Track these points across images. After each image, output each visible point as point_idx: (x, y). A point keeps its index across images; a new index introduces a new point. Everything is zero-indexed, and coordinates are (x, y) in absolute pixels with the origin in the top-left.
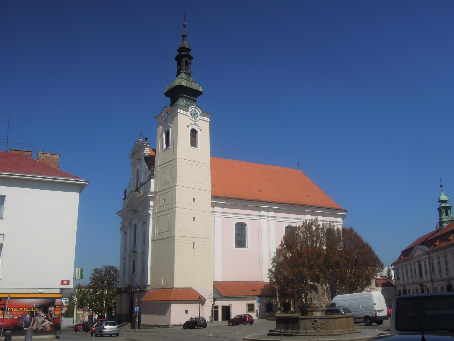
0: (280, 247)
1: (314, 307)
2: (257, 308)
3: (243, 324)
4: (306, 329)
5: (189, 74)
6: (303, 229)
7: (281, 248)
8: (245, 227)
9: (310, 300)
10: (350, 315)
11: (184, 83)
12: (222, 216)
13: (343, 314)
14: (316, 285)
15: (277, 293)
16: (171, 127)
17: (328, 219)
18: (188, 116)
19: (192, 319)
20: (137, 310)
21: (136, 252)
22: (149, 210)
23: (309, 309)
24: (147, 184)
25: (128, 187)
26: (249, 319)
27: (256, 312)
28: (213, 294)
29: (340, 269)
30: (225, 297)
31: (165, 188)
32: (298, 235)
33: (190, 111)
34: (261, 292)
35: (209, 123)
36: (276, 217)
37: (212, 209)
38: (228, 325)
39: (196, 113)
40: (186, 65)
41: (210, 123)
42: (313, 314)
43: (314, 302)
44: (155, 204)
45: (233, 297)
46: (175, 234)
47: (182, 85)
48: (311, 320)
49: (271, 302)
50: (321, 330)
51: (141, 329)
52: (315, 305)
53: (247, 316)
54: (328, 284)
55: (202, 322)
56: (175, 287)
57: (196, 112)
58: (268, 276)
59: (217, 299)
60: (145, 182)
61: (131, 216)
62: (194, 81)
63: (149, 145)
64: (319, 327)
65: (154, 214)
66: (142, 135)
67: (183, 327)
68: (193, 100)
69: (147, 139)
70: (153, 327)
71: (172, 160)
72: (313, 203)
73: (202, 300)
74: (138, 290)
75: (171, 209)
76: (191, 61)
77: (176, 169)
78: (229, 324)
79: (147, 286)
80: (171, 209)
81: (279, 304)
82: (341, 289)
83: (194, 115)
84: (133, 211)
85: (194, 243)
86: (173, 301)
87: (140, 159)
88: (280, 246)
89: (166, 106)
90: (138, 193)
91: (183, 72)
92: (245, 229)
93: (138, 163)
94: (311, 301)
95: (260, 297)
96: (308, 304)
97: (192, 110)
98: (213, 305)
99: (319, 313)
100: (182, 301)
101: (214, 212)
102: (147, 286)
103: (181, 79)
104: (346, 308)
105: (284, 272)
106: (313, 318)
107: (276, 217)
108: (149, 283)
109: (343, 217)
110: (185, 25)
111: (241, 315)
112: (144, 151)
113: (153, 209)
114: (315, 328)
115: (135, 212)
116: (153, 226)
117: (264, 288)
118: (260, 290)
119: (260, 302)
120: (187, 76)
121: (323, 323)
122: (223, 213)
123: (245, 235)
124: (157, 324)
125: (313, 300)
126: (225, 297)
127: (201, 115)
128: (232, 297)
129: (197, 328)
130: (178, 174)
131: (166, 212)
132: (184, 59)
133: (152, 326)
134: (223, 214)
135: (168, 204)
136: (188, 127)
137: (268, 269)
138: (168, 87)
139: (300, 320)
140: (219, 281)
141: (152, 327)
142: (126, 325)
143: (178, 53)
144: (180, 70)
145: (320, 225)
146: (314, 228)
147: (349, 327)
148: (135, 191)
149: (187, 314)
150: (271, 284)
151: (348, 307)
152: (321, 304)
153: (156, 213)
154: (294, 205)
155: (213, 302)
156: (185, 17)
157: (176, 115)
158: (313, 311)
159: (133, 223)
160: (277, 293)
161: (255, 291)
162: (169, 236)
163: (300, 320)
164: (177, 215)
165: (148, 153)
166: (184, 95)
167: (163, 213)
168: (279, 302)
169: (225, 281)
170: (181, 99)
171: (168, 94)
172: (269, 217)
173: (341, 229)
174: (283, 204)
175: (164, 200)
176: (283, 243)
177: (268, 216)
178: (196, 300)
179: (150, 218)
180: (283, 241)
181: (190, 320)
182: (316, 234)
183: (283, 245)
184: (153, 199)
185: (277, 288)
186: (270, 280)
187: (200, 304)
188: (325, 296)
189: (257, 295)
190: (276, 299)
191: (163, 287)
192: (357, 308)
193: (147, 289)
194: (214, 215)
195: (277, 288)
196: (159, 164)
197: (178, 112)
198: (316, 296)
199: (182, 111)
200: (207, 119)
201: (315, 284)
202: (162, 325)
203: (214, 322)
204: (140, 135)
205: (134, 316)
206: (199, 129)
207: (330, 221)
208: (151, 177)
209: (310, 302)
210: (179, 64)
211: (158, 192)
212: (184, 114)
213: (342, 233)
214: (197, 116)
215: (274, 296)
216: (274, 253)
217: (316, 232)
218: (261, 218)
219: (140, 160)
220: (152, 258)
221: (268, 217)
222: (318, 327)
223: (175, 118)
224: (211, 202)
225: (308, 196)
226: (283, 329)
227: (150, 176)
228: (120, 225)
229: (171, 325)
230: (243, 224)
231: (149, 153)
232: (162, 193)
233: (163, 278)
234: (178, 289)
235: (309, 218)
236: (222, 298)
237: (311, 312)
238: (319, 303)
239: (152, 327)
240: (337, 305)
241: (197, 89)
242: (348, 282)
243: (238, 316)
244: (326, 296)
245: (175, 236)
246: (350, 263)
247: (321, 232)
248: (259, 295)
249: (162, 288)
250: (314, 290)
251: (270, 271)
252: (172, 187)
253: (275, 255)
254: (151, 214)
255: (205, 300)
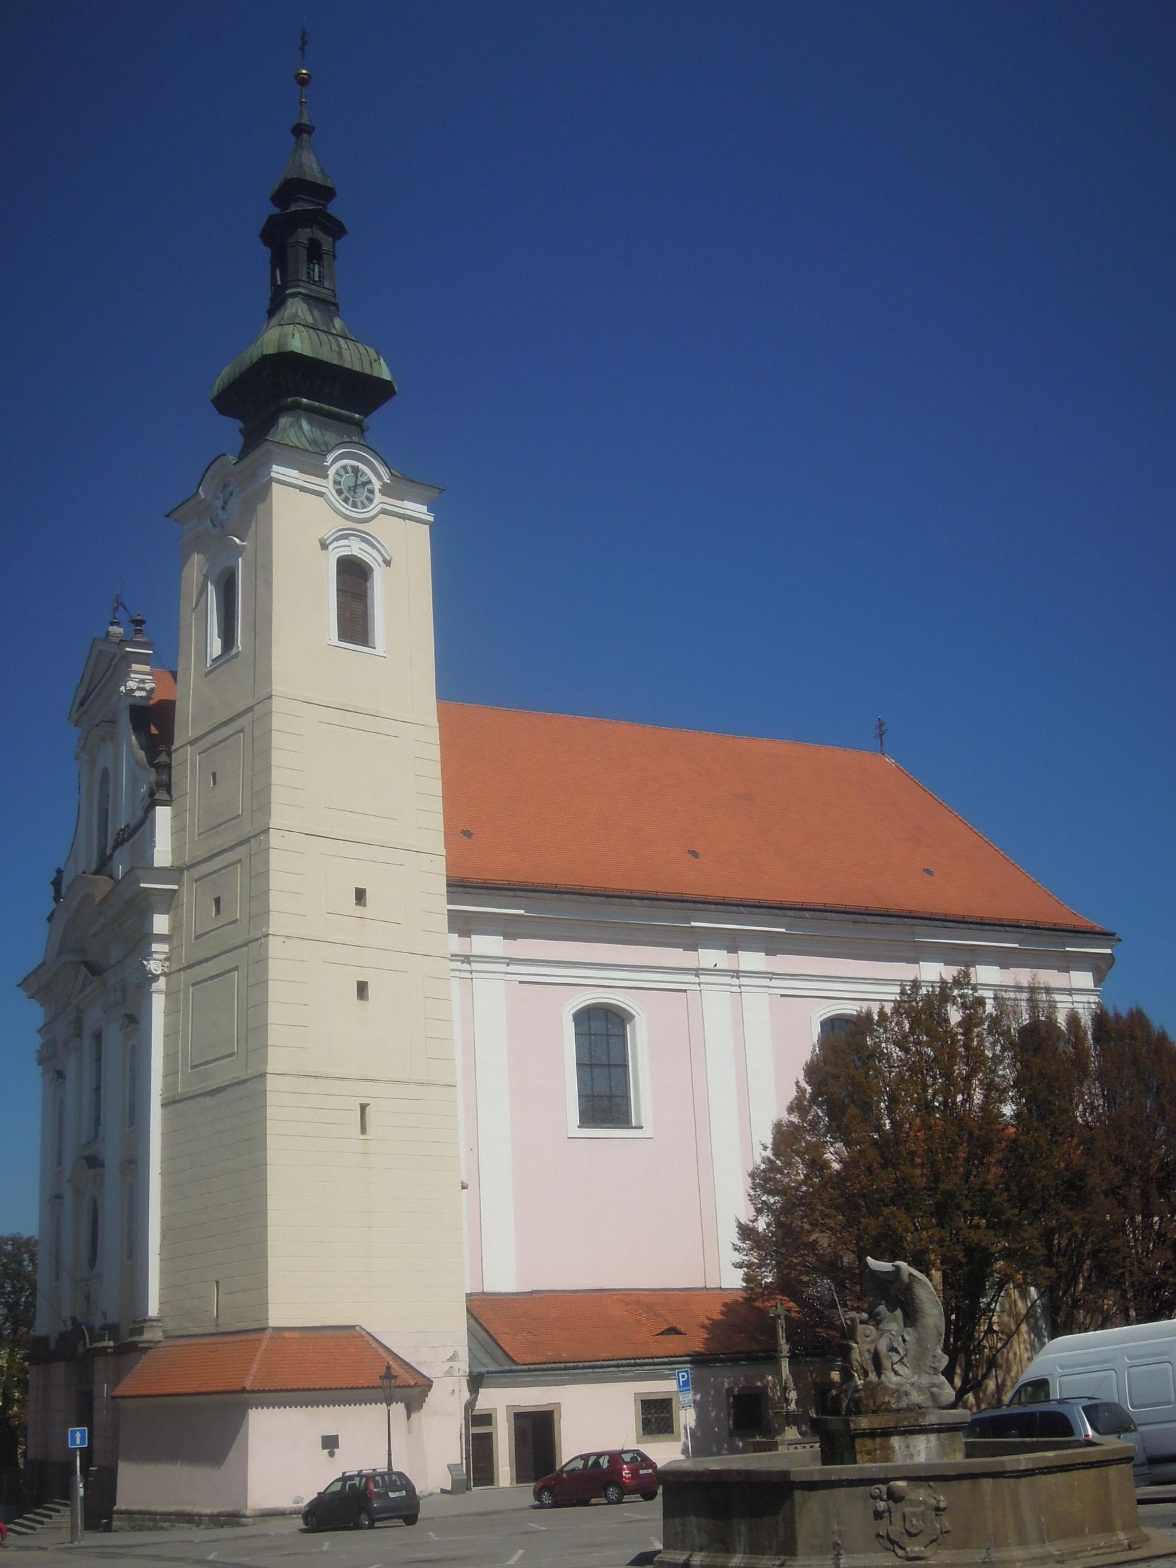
0: (789, 1113)
1: (894, 1406)
2: (686, 1417)
3: (606, 1497)
4: (836, 1546)
5: (326, 305)
6: (899, 1024)
7: (795, 1119)
8: (624, 1029)
9: (870, 1367)
10: (1115, 1451)
11: (299, 343)
12: (509, 977)
13: (1089, 1443)
14: (905, 1278)
15: (783, 1341)
16: (239, 551)
17: (1023, 976)
18: (321, 494)
19: (344, 1479)
20: (78, 1442)
21: (101, 1164)
22: (149, 955)
23: (864, 1423)
24: (139, 833)
25: (68, 859)
26: (634, 1472)
27: (683, 1439)
28: (464, 1355)
29: (1089, 1208)
30: (525, 1367)
31: (219, 842)
32: (876, 1053)
33: (331, 472)
34: (707, 1339)
35: (428, 526)
36: (772, 975)
37: (455, 943)
38: (534, 1507)
39: (364, 484)
40: (310, 260)
41: (435, 529)
42: (892, 1449)
43: (895, 1379)
44: (175, 927)
45: (566, 1369)
46: (266, 1063)
47: (293, 353)
48: (868, 1489)
49: (759, 1384)
50: (928, 1552)
51: (115, 1531)
52: (898, 1393)
53: (627, 1458)
54: (1032, 1289)
55: (392, 1495)
56: (270, 1325)
57: (364, 479)
58: (738, 1257)
59: (485, 1381)
60: (133, 823)
61: (81, 992)
62: (349, 336)
63: (151, 652)
64: (916, 1535)
65: (174, 972)
66: (120, 606)
67: (306, 1524)
68: (349, 421)
69: (140, 623)
70: (170, 1521)
71: (250, 709)
72: (953, 902)
73: (410, 1386)
74: (111, 1344)
75: (246, 945)
76: (334, 241)
77: (267, 751)
78: (537, 1503)
79: (145, 1321)
80: (246, 945)
81: (793, 1395)
82: (1100, 1309)
83: (354, 489)
84: (84, 971)
85: (363, 1108)
86: (259, 1391)
87: (112, 722)
88: (790, 1110)
89: (219, 457)
90: (107, 878)
91: (300, 293)
92: (624, 1036)
93: (103, 739)
94: (879, 1374)
95: (698, 1360)
96: (857, 1390)
97: (344, 468)
98: (470, 1405)
99: (928, 1441)
100: (304, 1390)
101: (467, 959)
102: (145, 1321)
103: (286, 327)
104: (1109, 1406)
105: (813, 1237)
106: (882, 1476)
107: (772, 975)
108: (153, 1310)
109: (1101, 968)
110: (303, 82)
111: (599, 1455)
112: (125, 678)
113: (167, 951)
114: (893, 1542)
115: (95, 970)
116: (171, 1034)
117: (720, 1317)
118: (703, 1327)
119: (697, 1385)
120: (316, 312)
121: (944, 1509)
122: (511, 961)
123: (626, 1066)
124: (188, 1508)
125: (887, 1363)
126: (525, 1367)
127: (386, 490)
128: (562, 1365)
129: (371, 1527)
130: (277, 776)
131: (225, 962)
132: (303, 235)
133: (166, 1516)
134: (513, 968)
135: (235, 921)
136: (324, 546)
137: (736, 1224)
138: (226, 371)
139: (798, 1494)
140: (502, 1290)
141: (167, 1525)
142: (58, 1511)
143: (276, 211)
144: (285, 286)
145: (981, 1002)
146: (955, 1016)
147: (1106, 1526)
148: (95, 873)
149: (332, 1454)
150: (755, 1300)
151: (1117, 1402)
152: (935, 1390)
153: (179, 970)
154: (858, 917)
155: (466, 1395)
156: (305, 43)
157: (264, 493)
158: (886, 1433)
159: (89, 1025)
160: (783, 1341)
161: (678, 1332)
162: (243, 1075)
163: (798, 1494)
164: (275, 969)
165: (148, 686)
166: (304, 400)
167: (211, 968)
168: (791, 1385)
169: (532, 1292)
170: (291, 419)
171: (226, 402)
172: (738, 978)
173: (1086, 1020)
174: (807, 914)
175: (217, 901)
176: (807, 1096)
177: (737, 972)
178: (373, 1387)
179: (154, 995)
180: (803, 1084)
181: (338, 1487)
182: (967, 1046)
183: (806, 1103)
184: (168, 901)
185: (778, 1316)
186: (744, 1280)
187: (389, 1405)
188: (1022, 1346)
189: (688, 1355)
190: (778, 1373)
191: (217, 1325)
192: (1169, 1403)
193: (147, 1336)
194: (471, 972)
195: (778, 1316)
196: (191, 734)
197: (272, 480)
198: (904, 1341)
199: (295, 473)
200: (420, 510)
201: (898, 1268)
202: (208, 1511)
203: (474, 1489)
204: (115, 610)
205: (94, 1468)
206: (380, 559)
207: (1033, 990)
208: (157, 796)
209: (873, 1377)
210: (280, 260)
211: (189, 868)
212: (302, 489)
213: (1094, 1038)
214: (341, 476)
215: (770, 1357)
216: (765, 1148)
217: (967, 1033)
218: (699, 984)
219: (114, 722)
220: (165, 1188)
221: (737, 974)
222: (913, 1530)
223: (261, 508)
224: (448, 910)
225: (928, 871)
226: (701, 1549)
227: (152, 794)
228: (38, 1041)
229: (248, 1512)
230: (615, 1014)
231: (152, 690)
232: (206, 868)
233: (217, 1283)
234: (287, 1334)
235: (932, 972)
236: (510, 1371)
237: (878, 1440)
238: (925, 1380)
239: (165, 1521)
240: (1056, 1393)
241: (367, 371)
242: (1131, 1273)
243: (581, 1457)
244: (1026, 1349)
245: (268, 1075)
246: (1135, 1181)
247: (990, 1033)
248: (699, 1354)
249: (213, 1330)
250: (892, 1310)
251: (746, 1232)
252: (248, 840)
253: (769, 1153)
254: (159, 972)
255: (425, 1385)
